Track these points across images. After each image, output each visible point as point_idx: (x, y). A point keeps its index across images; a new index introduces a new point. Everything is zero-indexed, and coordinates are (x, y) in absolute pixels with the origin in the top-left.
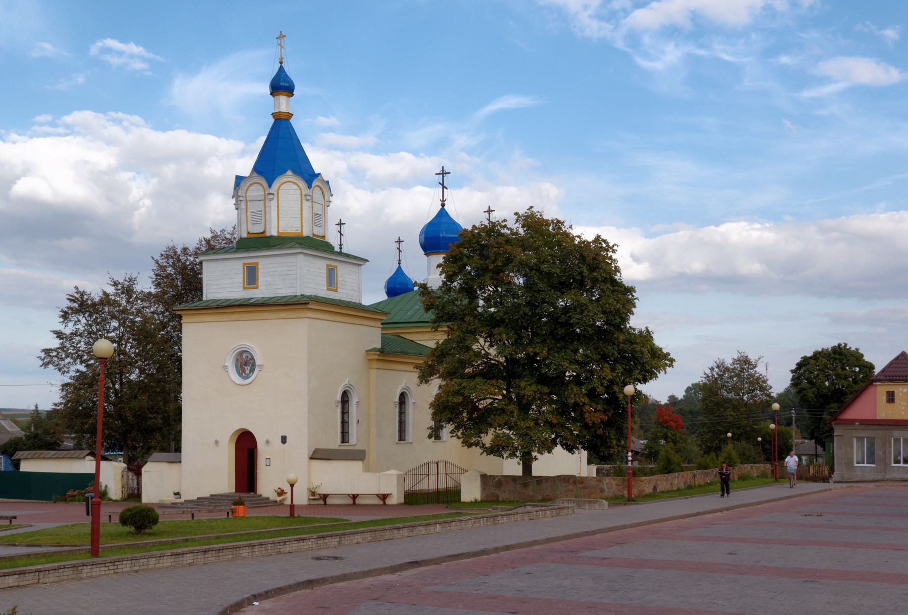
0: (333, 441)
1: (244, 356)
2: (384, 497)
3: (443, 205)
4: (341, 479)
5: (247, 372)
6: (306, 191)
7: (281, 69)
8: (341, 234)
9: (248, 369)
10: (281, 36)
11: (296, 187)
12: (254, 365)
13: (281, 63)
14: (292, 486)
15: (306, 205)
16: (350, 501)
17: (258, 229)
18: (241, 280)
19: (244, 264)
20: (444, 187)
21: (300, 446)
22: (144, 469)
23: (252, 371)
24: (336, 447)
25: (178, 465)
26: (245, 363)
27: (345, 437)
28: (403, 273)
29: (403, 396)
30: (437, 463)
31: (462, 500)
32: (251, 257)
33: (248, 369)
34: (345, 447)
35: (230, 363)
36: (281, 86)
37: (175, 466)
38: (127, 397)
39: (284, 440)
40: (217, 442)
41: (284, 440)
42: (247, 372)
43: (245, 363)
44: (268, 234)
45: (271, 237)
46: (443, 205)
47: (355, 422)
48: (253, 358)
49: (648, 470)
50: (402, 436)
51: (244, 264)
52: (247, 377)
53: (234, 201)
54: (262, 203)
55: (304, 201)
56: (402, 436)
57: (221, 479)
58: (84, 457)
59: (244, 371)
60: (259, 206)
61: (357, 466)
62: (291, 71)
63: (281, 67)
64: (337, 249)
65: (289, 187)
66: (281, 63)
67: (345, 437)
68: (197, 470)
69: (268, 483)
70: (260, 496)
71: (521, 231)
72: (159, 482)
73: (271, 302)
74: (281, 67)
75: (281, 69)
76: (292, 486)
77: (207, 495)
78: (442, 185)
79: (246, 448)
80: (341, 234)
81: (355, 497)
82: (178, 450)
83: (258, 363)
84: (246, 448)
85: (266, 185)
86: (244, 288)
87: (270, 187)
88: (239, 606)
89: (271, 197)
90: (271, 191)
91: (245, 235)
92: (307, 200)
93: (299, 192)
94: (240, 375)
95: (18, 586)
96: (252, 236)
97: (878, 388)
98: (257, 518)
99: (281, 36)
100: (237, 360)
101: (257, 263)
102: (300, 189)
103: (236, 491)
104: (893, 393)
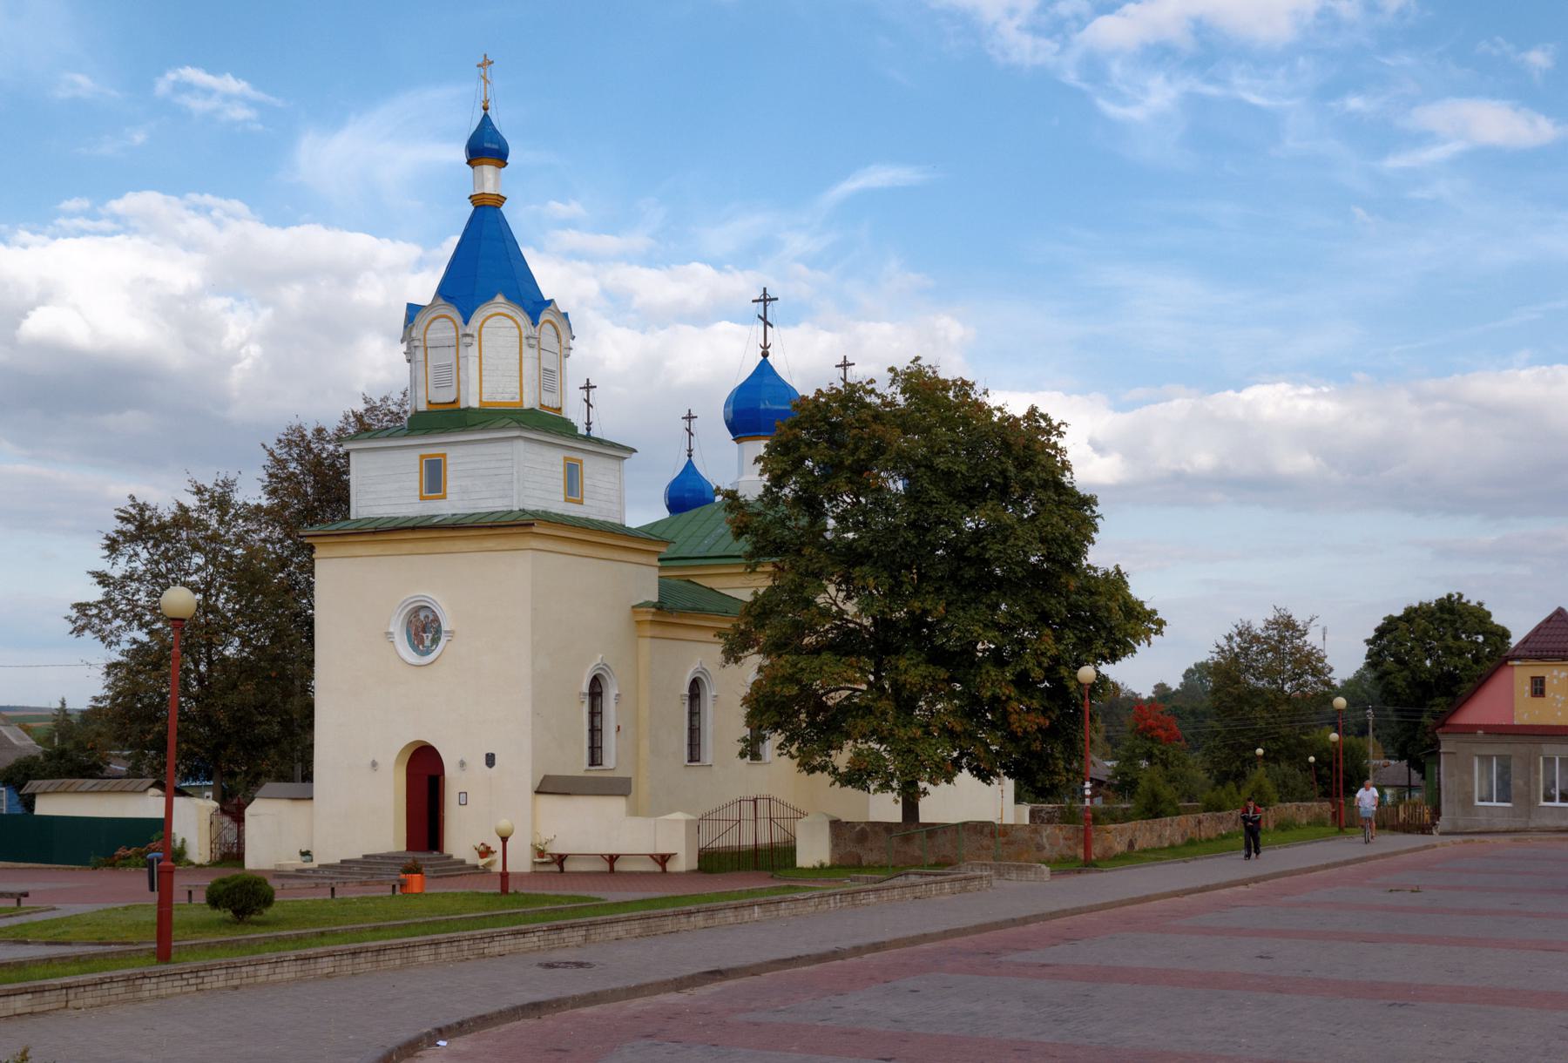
1: (422, 615)
2: (663, 859)
3: (765, 355)
5: (427, 643)
6: (528, 329)
7: (486, 119)
8: (589, 405)
10: (486, 63)
11: (511, 323)
13: (486, 109)
14: (504, 840)
15: (529, 354)
16: (605, 867)
17: (445, 396)
18: (449, 468)
19: (422, 457)
20: (766, 323)
21: (519, 772)
23: (435, 641)
24: (581, 773)
25: (308, 803)
26: (424, 628)
27: (595, 758)
28: (696, 472)
31: (799, 865)
32: (433, 445)
34: (595, 772)
35: (397, 628)
36: (486, 148)
37: (302, 806)
38: (220, 687)
39: (490, 760)
40: (374, 764)
41: (490, 760)
42: (427, 643)
43: (424, 628)
44: (463, 405)
45: (468, 409)
46: (765, 355)
47: (614, 730)
48: (436, 619)
49: (1119, 813)
50: (694, 754)
51: (422, 457)
52: (427, 652)
53: (404, 347)
54: (453, 350)
55: (525, 347)
56: (694, 754)
57: (381, 828)
58: (146, 791)
60: (448, 357)
61: (616, 805)
62: (503, 122)
63: (486, 115)
64: (582, 431)
65: (498, 324)
66: (486, 109)
67: (595, 758)
68: (341, 812)
69: (462, 836)
70: (450, 857)
72: (275, 833)
73: (469, 521)
74: (486, 115)
75: (486, 119)
76: (504, 840)
78: (764, 319)
79: (425, 774)
80: (589, 405)
81: (612, 859)
82: (308, 777)
84: (425, 774)
85: (459, 319)
86: (422, 498)
87: (466, 322)
89: (468, 340)
91: (422, 407)
92: (531, 346)
93: (516, 332)
94: (415, 648)
96: (434, 408)
97: (1516, 670)
99: (486, 63)
101: (444, 455)
103: (408, 849)
104: (1542, 679)
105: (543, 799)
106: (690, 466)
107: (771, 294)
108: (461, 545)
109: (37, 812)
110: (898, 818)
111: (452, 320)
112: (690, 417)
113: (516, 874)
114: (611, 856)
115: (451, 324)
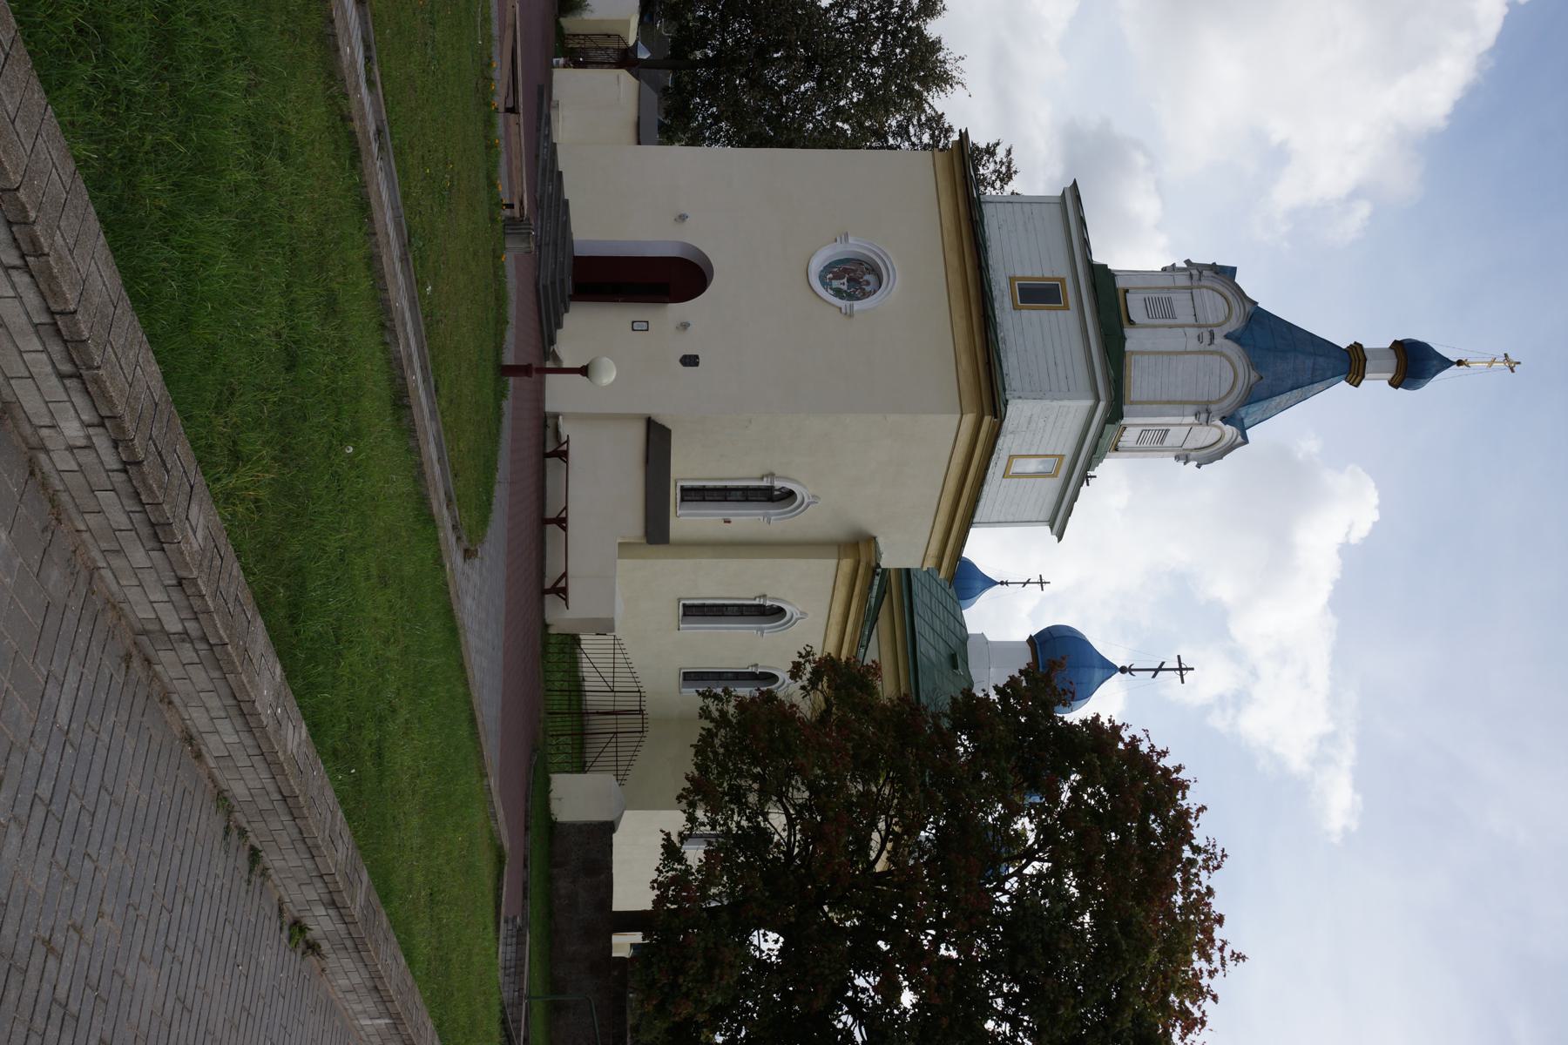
0: (685, 469)
2: (561, 591)
3: (1123, 670)
4: (600, 485)
5: (836, 284)
7: (1446, 363)
9: (842, 284)
11: (1224, 393)
12: (851, 297)
13: (1460, 363)
14: (584, 371)
16: (551, 513)
18: (1028, 274)
20: (1160, 669)
22: (624, 74)
23: (838, 293)
24: (674, 474)
26: (854, 277)
27: (695, 495)
28: (983, 590)
29: (778, 612)
30: (641, 712)
32: (1077, 293)
33: (842, 284)
34: (675, 494)
35: (855, 246)
36: (1414, 363)
37: (629, 132)
39: (690, 361)
40: (683, 218)
41: (690, 361)
43: (854, 277)
44: (1128, 332)
45: (1123, 339)
46: (1123, 670)
48: (865, 295)
50: (694, 611)
51: (1062, 280)
52: (822, 279)
54: (1191, 320)
56: (694, 611)
59: (837, 277)
62: (1442, 381)
63: (1452, 363)
64: (1090, 473)
65: (1225, 371)
66: (1460, 363)
67: (695, 495)
69: (587, 330)
71: (1195, 956)
72: (594, 112)
73: (991, 335)
74: (1452, 363)
75: (1446, 363)
76: (584, 371)
77: (568, 193)
79: (674, 278)
81: (561, 522)
83: (858, 305)
84: (674, 278)
85: (1228, 328)
87: (1227, 337)
88: (18, 223)
90: (1219, 340)
93: (1215, 397)
94: (828, 268)
95: (537, 156)
98: (384, 308)
100: (860, 262)
101: (1066, 308)
102: (1221, 400)
103: (576, 258)
105: (637, 433)
106: (991, 583)
107: (1188, 675)
108: (961, 325)
109: (615, 908)
110: (618, 905)
111: (1228, 318)
112: (1041, 583)
113: (542, 384)
114: (565, 520)
115: (1221, 319)
